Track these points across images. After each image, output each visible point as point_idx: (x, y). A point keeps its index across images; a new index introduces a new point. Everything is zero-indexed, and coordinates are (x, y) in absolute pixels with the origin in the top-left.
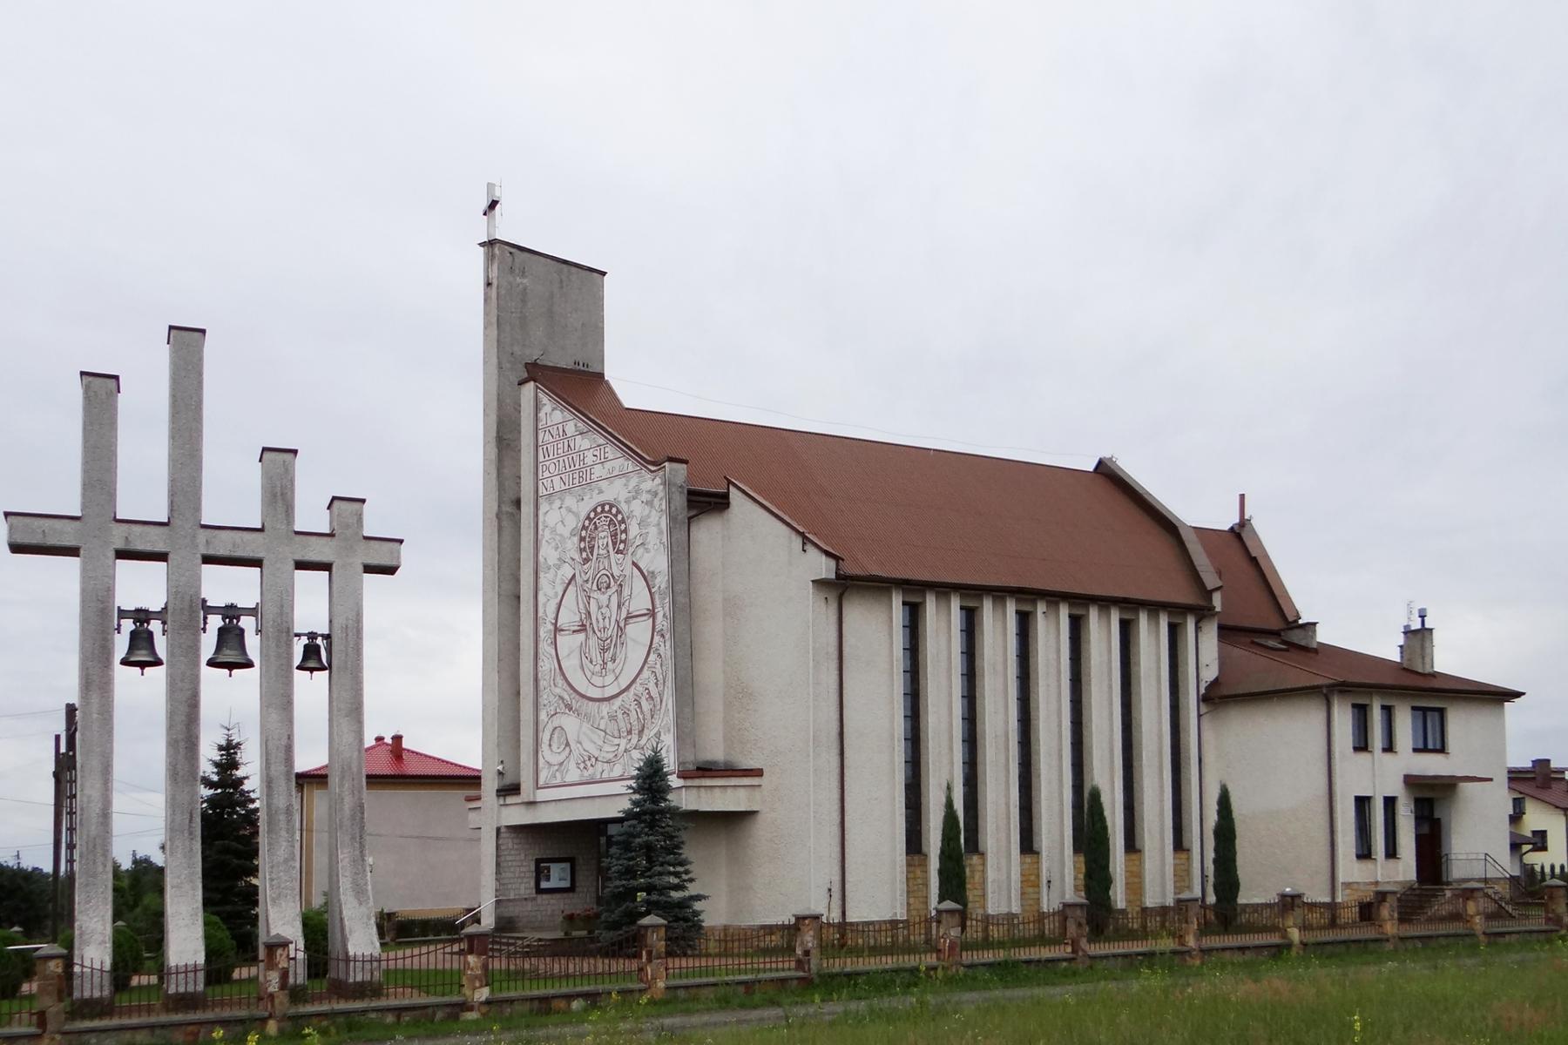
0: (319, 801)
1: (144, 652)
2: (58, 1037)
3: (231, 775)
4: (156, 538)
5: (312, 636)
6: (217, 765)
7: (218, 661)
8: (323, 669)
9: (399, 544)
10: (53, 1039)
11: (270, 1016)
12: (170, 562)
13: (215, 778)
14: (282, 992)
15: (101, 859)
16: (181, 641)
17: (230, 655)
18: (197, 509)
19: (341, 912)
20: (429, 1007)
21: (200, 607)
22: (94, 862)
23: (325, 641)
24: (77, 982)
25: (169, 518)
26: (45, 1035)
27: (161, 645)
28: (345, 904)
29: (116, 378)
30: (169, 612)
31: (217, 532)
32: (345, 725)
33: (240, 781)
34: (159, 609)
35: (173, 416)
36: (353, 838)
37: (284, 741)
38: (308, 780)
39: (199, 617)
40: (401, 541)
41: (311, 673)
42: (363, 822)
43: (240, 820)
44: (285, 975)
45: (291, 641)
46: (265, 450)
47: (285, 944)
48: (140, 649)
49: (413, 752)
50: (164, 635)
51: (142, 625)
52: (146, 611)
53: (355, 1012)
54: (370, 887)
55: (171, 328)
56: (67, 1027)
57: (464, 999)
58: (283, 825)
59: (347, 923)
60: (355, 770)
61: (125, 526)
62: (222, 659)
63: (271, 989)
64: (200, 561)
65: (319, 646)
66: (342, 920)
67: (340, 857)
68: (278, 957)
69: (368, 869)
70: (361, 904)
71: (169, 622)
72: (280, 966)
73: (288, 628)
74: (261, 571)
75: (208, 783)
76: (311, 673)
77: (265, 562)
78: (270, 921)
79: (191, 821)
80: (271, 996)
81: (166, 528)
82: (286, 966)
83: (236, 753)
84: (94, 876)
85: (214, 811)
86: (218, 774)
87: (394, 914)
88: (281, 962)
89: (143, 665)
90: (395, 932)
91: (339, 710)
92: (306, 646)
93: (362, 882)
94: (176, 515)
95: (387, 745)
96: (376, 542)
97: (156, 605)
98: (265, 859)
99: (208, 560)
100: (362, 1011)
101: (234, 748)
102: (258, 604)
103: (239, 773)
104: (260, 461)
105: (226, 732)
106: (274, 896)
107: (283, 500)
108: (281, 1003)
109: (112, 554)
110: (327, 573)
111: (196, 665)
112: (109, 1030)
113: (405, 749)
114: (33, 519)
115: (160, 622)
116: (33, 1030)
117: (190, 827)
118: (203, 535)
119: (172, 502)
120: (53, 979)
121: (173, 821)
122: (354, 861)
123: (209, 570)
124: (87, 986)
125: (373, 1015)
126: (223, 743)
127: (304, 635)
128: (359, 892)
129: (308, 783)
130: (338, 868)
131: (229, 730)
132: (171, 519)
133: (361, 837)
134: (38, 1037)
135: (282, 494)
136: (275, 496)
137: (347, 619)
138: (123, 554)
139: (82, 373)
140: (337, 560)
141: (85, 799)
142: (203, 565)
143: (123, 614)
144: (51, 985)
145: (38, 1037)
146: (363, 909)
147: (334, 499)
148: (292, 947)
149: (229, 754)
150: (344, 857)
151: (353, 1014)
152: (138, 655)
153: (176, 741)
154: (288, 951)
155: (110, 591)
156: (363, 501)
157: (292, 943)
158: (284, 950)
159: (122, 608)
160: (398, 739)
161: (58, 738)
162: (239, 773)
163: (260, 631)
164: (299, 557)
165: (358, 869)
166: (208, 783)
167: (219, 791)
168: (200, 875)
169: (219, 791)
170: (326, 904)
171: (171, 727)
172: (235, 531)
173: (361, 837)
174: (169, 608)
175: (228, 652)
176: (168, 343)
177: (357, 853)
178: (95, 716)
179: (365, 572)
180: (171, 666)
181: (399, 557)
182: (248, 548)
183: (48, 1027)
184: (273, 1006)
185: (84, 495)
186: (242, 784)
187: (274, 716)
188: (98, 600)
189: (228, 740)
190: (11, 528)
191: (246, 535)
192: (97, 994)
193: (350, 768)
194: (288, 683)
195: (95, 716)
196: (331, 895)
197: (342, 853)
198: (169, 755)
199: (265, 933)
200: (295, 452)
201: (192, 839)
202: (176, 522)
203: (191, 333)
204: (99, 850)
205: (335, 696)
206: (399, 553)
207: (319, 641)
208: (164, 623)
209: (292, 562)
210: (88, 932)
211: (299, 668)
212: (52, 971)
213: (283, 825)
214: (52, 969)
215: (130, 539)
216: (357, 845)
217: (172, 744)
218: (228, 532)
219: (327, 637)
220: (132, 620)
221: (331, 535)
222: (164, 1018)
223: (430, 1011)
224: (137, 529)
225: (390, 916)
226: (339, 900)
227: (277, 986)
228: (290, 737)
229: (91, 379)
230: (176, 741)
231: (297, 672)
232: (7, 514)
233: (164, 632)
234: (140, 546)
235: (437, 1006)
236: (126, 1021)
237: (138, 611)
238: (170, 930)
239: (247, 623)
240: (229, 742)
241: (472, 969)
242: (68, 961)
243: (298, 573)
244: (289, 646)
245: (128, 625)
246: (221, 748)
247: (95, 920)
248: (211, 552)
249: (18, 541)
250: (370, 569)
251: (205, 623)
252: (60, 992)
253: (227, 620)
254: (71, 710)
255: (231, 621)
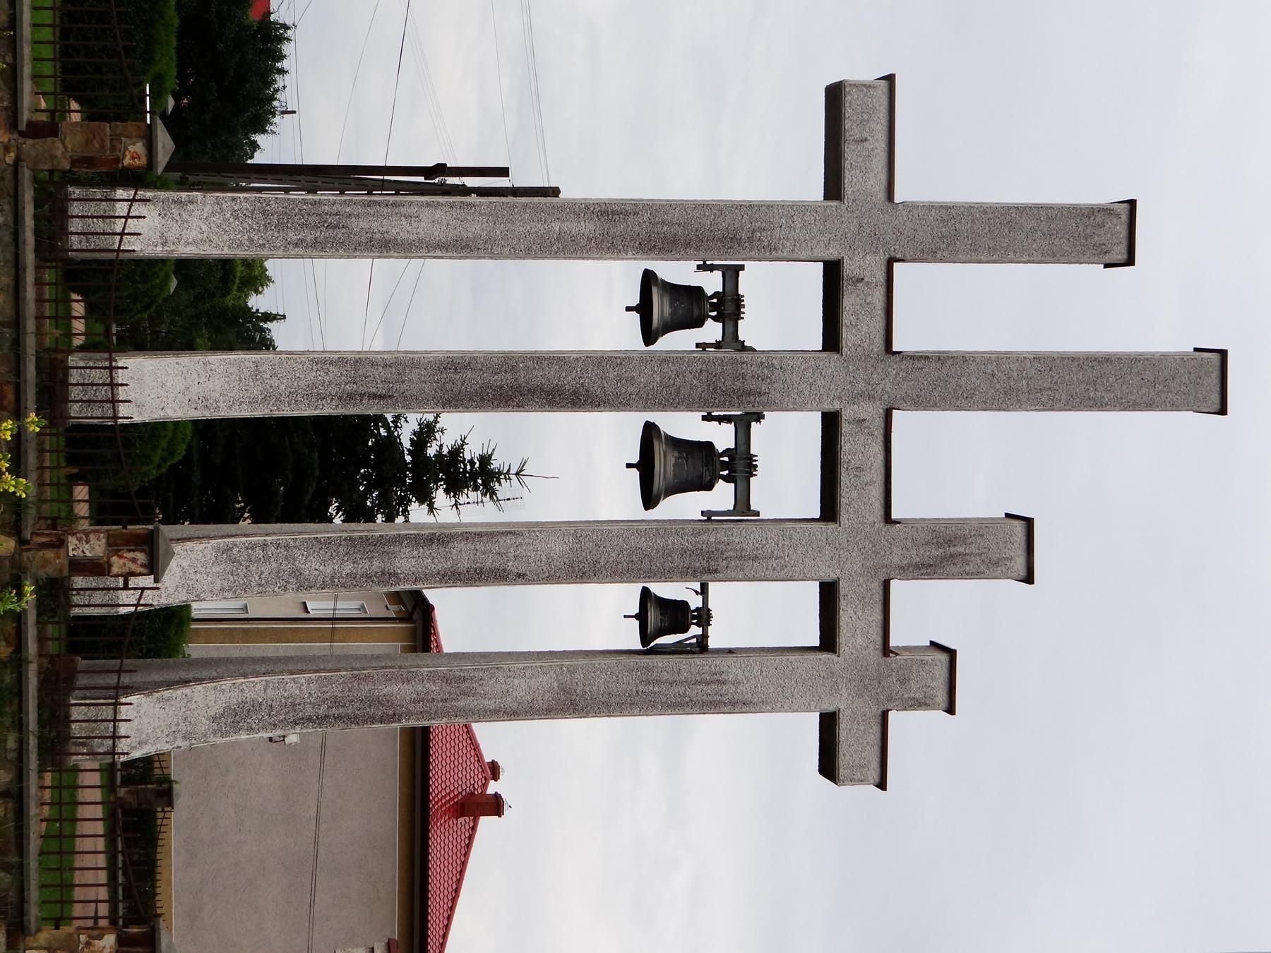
0: (386, 646)
1: (667, 310)
2: (11, 158)
3: (437, 481)
4: (865, 329)
5: (704, 617)
6: (456, 452)
7: (656, 443)
8: (645, 637)
9: (877, 780)
10: (7, 149)
11: (22, 542)
12: (824, 355)
13: (431, 451)
14: (66, 563)
15: (310, 238)
16: (689, 377)
17: (665, 465)
18: (919, 403)
19: (200, 681)
20: (21, 856)
21: (748, 410)
22: (304, 226)
23: (694, 641)
24: (98, 193)
25: (899, 353)
26: (16, 136)
27: (680, 341)
28: (215, 688)
29: (1130, 261)
30: (738, 355)
31: (879, 434)
32: (544, 683)
33: (426, 498)
34: (741, 338)
35: (1073, 359)
36: (336, 702)
37: (512, 566)
38: (420, 631)
39: (731, 406)
40: (882, 785)
41: (636, 617)
42: (365, 722)
43: (355, 497)
44: (97, 568)
45: (694, 577)
46: (1029, 523)
47: (154, 568)
48: (671, 305)
49: (471, 838)
50: (698, 345)
51: (714, 307)
52: (737, 315)
53: (21, 708)
54: (244, 736)
55: (1223, 354)
56: (26, 174)
57: (33, 927)
58: (364, 566)
59: (179, 692)
60: (461, 704)
61: (880, 276)
62: (659, 448)
63: (72, 541)
64: (828, 407)
65: (685, 630)
66: (186, 682)
67: (302, 678)
68: (131, 555)
69: (277, 733)
70: (214, 719)
71: (720, 354)
72: (114, 559)
73: (716, 571)
74: (813, 520)
75: (426, 433)
76: (636, 617)
77: (832, 526)
78: (189, 545)
79: (374, 396)
80: (60, 544)
81: (882, 347)
82: (115, 570)
83: (476, 489)
84: (281, 226)
85: (371, 449)
86: (439, 455)
87: (171, 804)
88: (121, 561)
89: (644, 309)
90: (135, 804)
91: (572, 671)
92: (684, 605)
93: (253, 720)
94: (904, 365)
95: (485, 786)
96: (878, 735)
97: (747, 332)
98: (300, 533)
99: (831, 423)
100: (20, 719)
101: (485, 484)
102: (757, 514)
103: (441, 497)
104: (1008, 515)
105: (513, 471)
106: (235, 550)
107: (944, 558)
108: (46, 562)
109: (832, 254)
110: (817, 644)
111: (645, 408)
112: (17, 247)
113: (476, 821)
114: (884, 121)
115: (720, 338)
116: (26, 116)
117: (362, 395)
118: (872, 412)
119: (927, 358)
120: (113, 148)
121: (373, 364)
122: (293, 704)
123: (813, 422)
124: (90, 209)
125: (11, 743)
126: (495, 465)
127: (705, 601)
128: (236, 717)
129: (415, 629)
130: (281, 673)
131: (517, 474)
132: (898, 358)
133: (338, 718)
134: (13, 121)
135: (952, 556)
136: (949, 542)
137: (737, 683)
138: (833, 275)
139: (1132, 204)
140: (841, 660)
141: (412, 211)
142: (819, 414)
143: (731, 274)
144: (103, 146)
145: (13, 121)
146: (204, 725)
147: (952, 653)
148: (148, 581)
149: (474, 475)
150: (299, 686)
151: (16, 701)
152: (662, 297)
153: (513, 369)
154: (141, 574)
155: (770, 252)
156: (951, 710)
157: (156, 581)
158: (142, 566)
159: (741, 273)
160: (495, 806)
161: (503, 172)
162: (441, 497)
163: (709, 519)
164: (844, 588)
165: (279, 713)
166: (426, 433)
167: (408, 459)
168: (277, 414)
169: (408, 459)
170: (893, 202)
171: (539, 359)
172: (882, 470)
173: (338, 718)
174: (745, 355)
175: (671, 460)
176: (1196, 350)
177: (309, 711)
178: (556, 226)
179: (821, 715)
180: (645, 359)
181: (852, 781)
182: (854, 494)
183: (30, 142)
184: (43, 546)
185: (930, 207)
186: (421, 501)
187: (558, 547)
188: (754, 231)
189: (500, 473)
190: (867, 86)
191: (876, 492)
192: (75, 226)
193: (465, 693)
194: (617, 574)
195: (556, 226)
196: (213, 670)
197: (309, 681)
198: (489, 356)
199: (173, 536)
200: (1029, 579)
201: (340, 398)
202: (892, 366)
203: (1217, 388)
204: (322, 235)
205: (597, 661)
206: (861, 781)
207: (695, 630)
208: (718, 345)
209: (833, 576)
210: (185, 215)
211: (646, 593)
212: (126, 148)
213: (364, 566)
214: (131, 148)
215: (860, 285)
216: (322, 710)
217: (509, 362)
218: (880, 458)
219: (702, 645)
220: (721, 290)
221: (886, 650)
222: (31, 343)
223: (13, 859)
224: (878, 297)
225: (166, 795)
226: (222, 678)
227: (78, 553)
228: (521, 578)
229: (1124, 218)
230: (513, 369)
231: (635, 589)
232: (890, 79)
233: (702, 346)
234: (849, 301)
235: (22, 874)
236: (30, 277)
237: (738, 301)
238: (180, 360)
239: (722, 496)
240: (496, 476)
241: (88, 944)
242: (139, 179)
243: (813, 589)
244: (683, 574)
245: (712, 283)
246: (485, 460)
247: (204, 227)
248: (845, 428)
249: (849, 98)
250: (828, 724)
251: (720, 419)
252: (89, 161)
253: (726, 459)
254: (555, 192)
255: (724, 466)
